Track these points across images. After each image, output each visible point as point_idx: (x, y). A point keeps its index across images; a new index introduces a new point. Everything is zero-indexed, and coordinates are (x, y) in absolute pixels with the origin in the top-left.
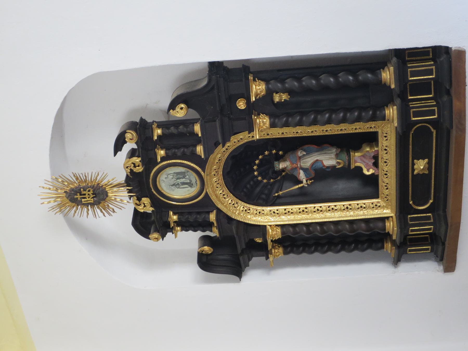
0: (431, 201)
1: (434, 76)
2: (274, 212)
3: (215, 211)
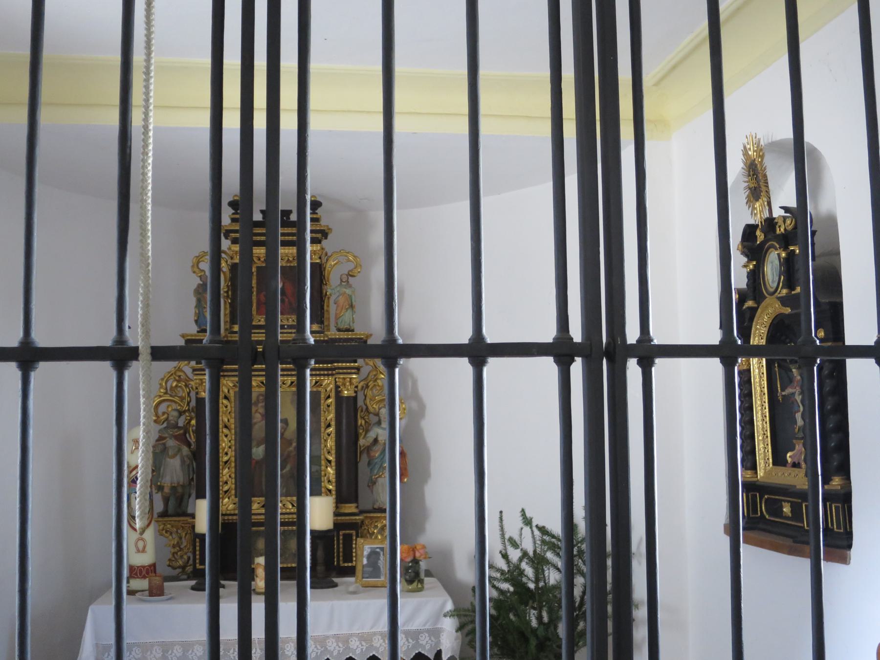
0: (767, 517)
1: (835, 530)
2: (760, 363)
3: (756, 305)
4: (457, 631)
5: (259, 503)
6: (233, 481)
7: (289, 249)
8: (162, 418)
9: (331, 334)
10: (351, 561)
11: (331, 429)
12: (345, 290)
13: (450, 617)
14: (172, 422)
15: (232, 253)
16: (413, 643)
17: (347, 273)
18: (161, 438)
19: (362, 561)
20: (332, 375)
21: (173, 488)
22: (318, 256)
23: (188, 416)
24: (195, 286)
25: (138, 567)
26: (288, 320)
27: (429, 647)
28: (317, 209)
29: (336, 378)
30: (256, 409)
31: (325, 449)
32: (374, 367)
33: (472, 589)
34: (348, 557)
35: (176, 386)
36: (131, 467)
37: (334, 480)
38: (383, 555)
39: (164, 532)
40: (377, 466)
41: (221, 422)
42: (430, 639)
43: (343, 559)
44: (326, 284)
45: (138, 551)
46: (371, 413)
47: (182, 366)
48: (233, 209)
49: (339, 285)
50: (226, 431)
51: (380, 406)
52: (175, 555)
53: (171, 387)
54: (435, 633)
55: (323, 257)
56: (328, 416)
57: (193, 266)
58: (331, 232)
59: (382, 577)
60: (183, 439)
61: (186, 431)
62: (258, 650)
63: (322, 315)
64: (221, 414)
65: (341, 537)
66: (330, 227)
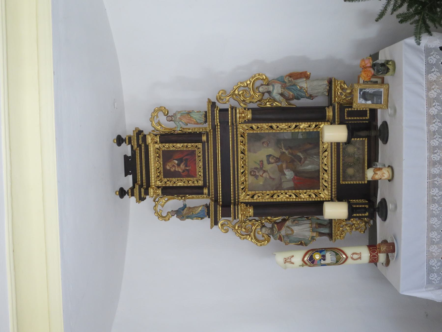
4: (431, 35)
5: (324, 174)
6: (308, 191)
7: (152, 180)
8: (266, 237)
9: (209, 127)
10: (366, 111)
11: (274, 125)
12: (178, 118)
13: (420, 40)
14: (269, 232)
15: (155, 195)
16: (435, 68)
17: (166, 117)
18: (280, 239)
19: (369, 105)
20: (236, 126)
21: (313, 231)
22: (155, 137)
23: (265, 221)
24: (178, 219)
25: (370, 258)
26: (199, 156)
27: (438, 56)
28: (123, 139)
29: (239, 123)
30: (260, 176)
31: (287, 129)
32: (231, 96)
33: (401, 23)
34: (362, 113)
35: (245, 229)
36: (303, 264)
37: (309, 123)
38: (365, 89)
39: (342, 236)
40: (300, 93)
41: (269, 200)
42: (432, 55)
43: (361, 117)
44: (173, 131)
45: (360, 258)
46: (262, 98)
47: (232, 225)
48: (125, 195)
49: (174, 122)
50: (275, 197)
51: (258, 91)
52: (357, 228)
53: (245, 232)
54: (428, 51)
55: (155, 133)
56: (265, 128)
57: (165, 220)
58: (138, 128)
59: (381, 90)
60: (281, 224)
61: (275, 223)
62: (435, 179)
63: (195, 133)
64: (264, 200)
65: (350, 118)
66: (134, 129)
